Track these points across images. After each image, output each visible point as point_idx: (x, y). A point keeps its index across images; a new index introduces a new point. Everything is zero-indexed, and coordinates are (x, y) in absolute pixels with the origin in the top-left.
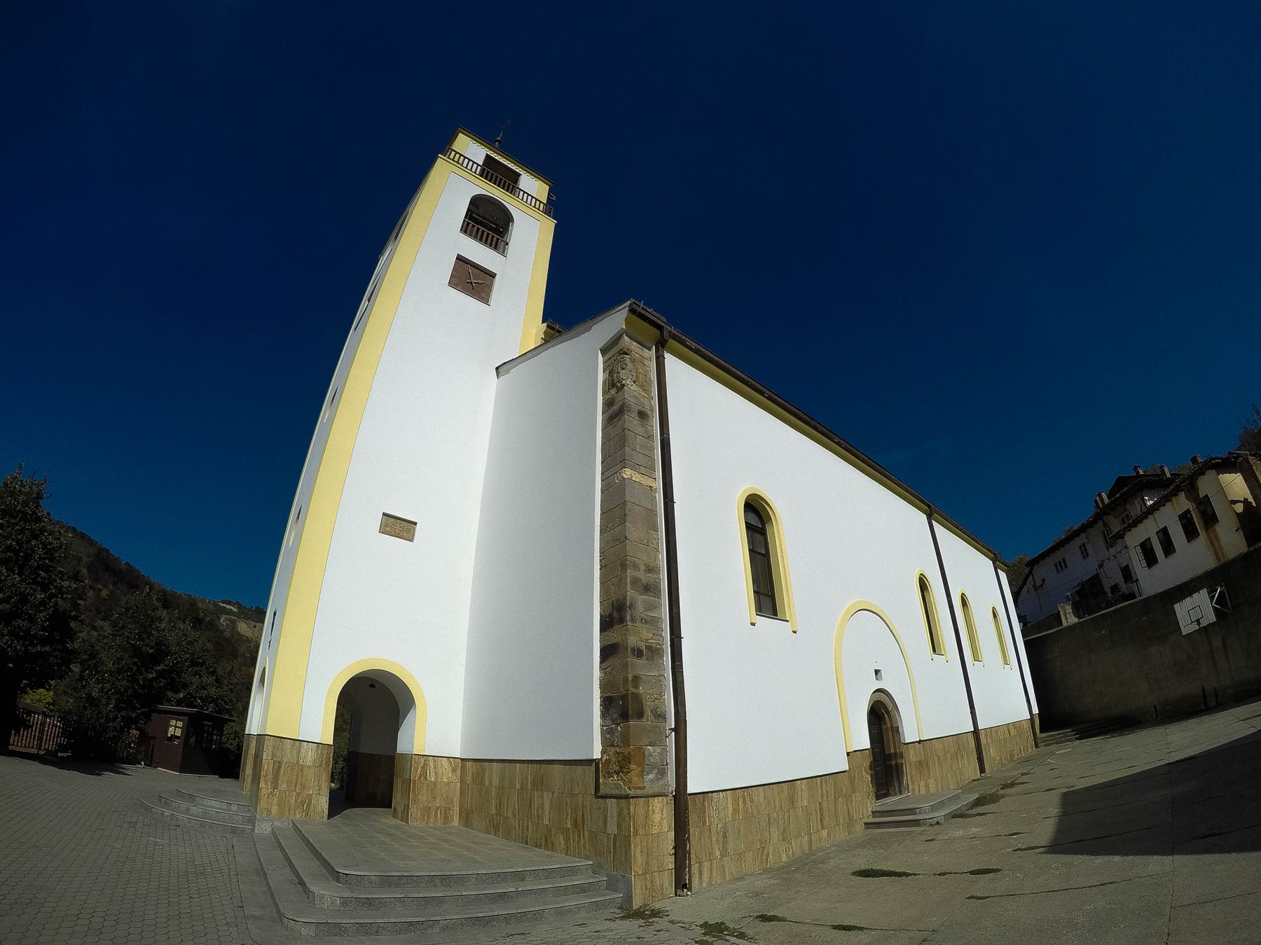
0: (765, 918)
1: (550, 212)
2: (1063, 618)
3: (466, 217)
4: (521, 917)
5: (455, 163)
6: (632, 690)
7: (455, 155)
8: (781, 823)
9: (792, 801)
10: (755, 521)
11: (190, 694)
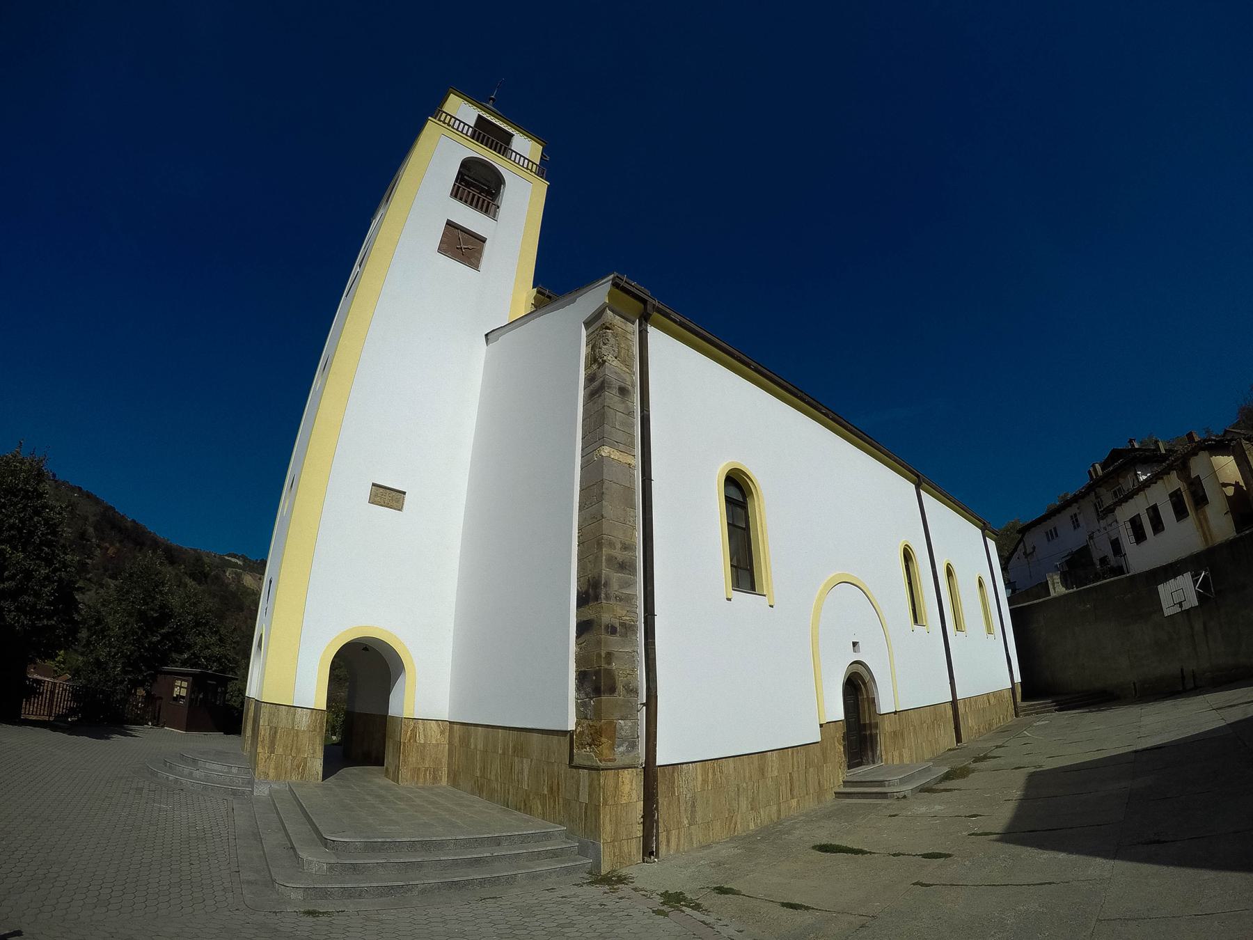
0: (721, 891)
1: (543, 174)
2: (1051, 587)
3: (456, 181)
4: (495, 881)
5: (446, 126)
6: (604, 666)
7: (446, 117)
8: (750, 793)
9: (762, 771)
10: (736, 495)
11: (194, 654)
